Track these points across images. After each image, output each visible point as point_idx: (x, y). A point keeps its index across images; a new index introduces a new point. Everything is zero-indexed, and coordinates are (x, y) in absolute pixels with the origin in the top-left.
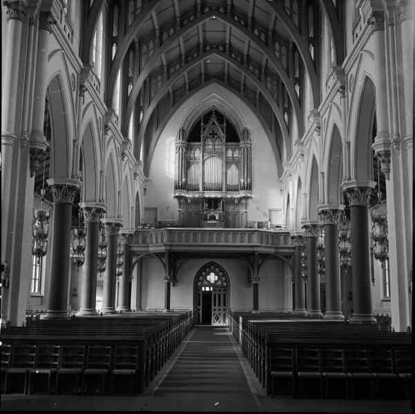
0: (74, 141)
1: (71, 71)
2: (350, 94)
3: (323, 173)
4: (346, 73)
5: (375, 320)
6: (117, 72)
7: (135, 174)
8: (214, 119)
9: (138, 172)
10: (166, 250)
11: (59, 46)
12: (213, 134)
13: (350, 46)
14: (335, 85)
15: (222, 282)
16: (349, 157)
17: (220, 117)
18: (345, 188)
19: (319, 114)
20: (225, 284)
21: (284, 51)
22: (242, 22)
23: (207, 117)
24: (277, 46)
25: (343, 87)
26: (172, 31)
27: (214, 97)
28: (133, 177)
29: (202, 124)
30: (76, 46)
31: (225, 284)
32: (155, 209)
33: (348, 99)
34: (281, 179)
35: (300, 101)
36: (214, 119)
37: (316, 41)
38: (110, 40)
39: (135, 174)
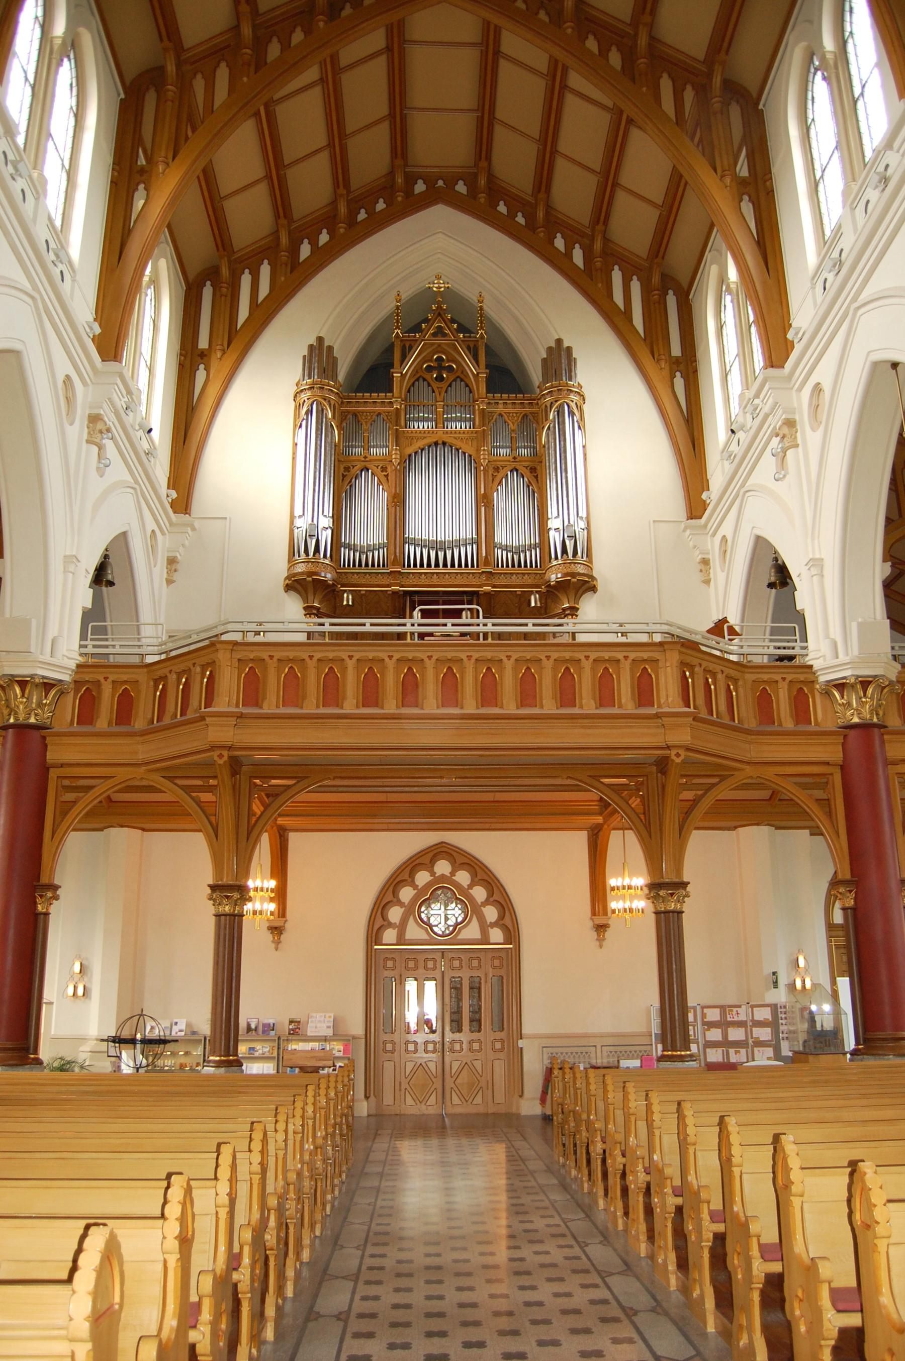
15: (484, 928)
22: (520, 219)
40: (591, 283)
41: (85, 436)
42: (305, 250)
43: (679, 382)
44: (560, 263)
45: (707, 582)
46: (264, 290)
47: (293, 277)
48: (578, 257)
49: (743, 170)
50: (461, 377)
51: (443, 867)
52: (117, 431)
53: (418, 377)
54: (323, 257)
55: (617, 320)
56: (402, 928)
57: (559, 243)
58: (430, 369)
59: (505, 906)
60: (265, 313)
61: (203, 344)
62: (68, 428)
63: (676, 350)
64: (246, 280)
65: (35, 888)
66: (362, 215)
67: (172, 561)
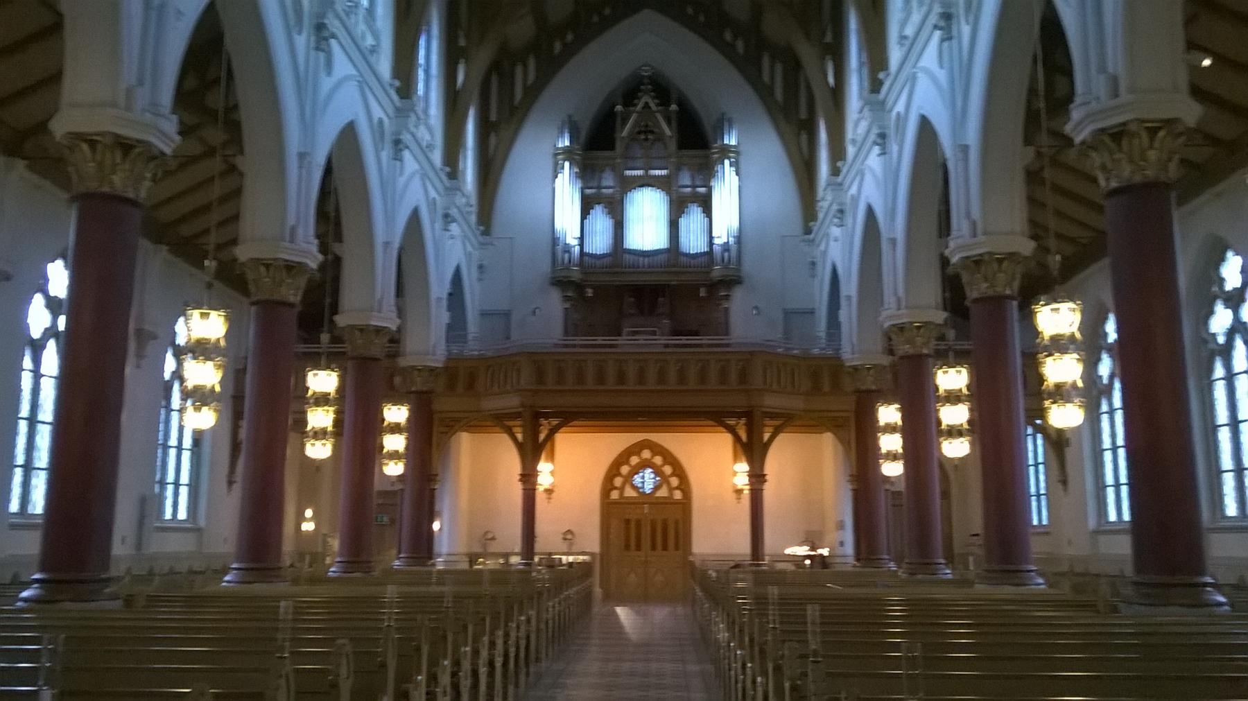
0: (302, 156)
1: (378, 113)
2: (895, 148)
3: (893, 242)
4: (888, 107)
5: (714, 575)
6: (465, 116)
7: (446, 216)
8: (646, 99)
9: (454, 212)
10: (522, 405)
11: (350, 66)
12: (646, 132)
13: (895, 54)
14: (868, 131)
15: (671, 489)
16: (894, 261)
17: (663, 91)
18: (886, 325)
19: (883, 103)
20: (678, 495)
21: (779, 68)
22: (702, 19)
23: (630, 94)
24: (766, 61)
25: (883, 136)
26: (570, 37)
27: (648, 43)
28: (439, 225)
29: (619, 108)
30: (385, 65)
31: (678, 495)
32: (507, 315)
33: (960, 43)
34: (840, 179)
35: (837, 95)
36: (646, 99)
37: (837, 52)
38: (452, 56)
39: (446, 216)
40: (748, 67)
41: (313, 44)
42: (558, 46)
43: (804, 137)
44: (726, 50)
45: (813, 276)
46: (532, 76)
47: (550, 66)
48: (740, 45)
49: (829, 38)
50: (660, 138)
51: (646, 454)
52: (341, 33)
53: (633, 138)
54: (570, 51)
55: (764, 93)
56: (622, 489)
57: (728, 36)
58: (639, 133)
59: (679, 472)
60: (533, 92)
61: (493, 117)
62: (296, 37)
63: (803, 115)
64: (519, 70)
65: (752, 418)
66: (596, 19)
67: (481, 267)
